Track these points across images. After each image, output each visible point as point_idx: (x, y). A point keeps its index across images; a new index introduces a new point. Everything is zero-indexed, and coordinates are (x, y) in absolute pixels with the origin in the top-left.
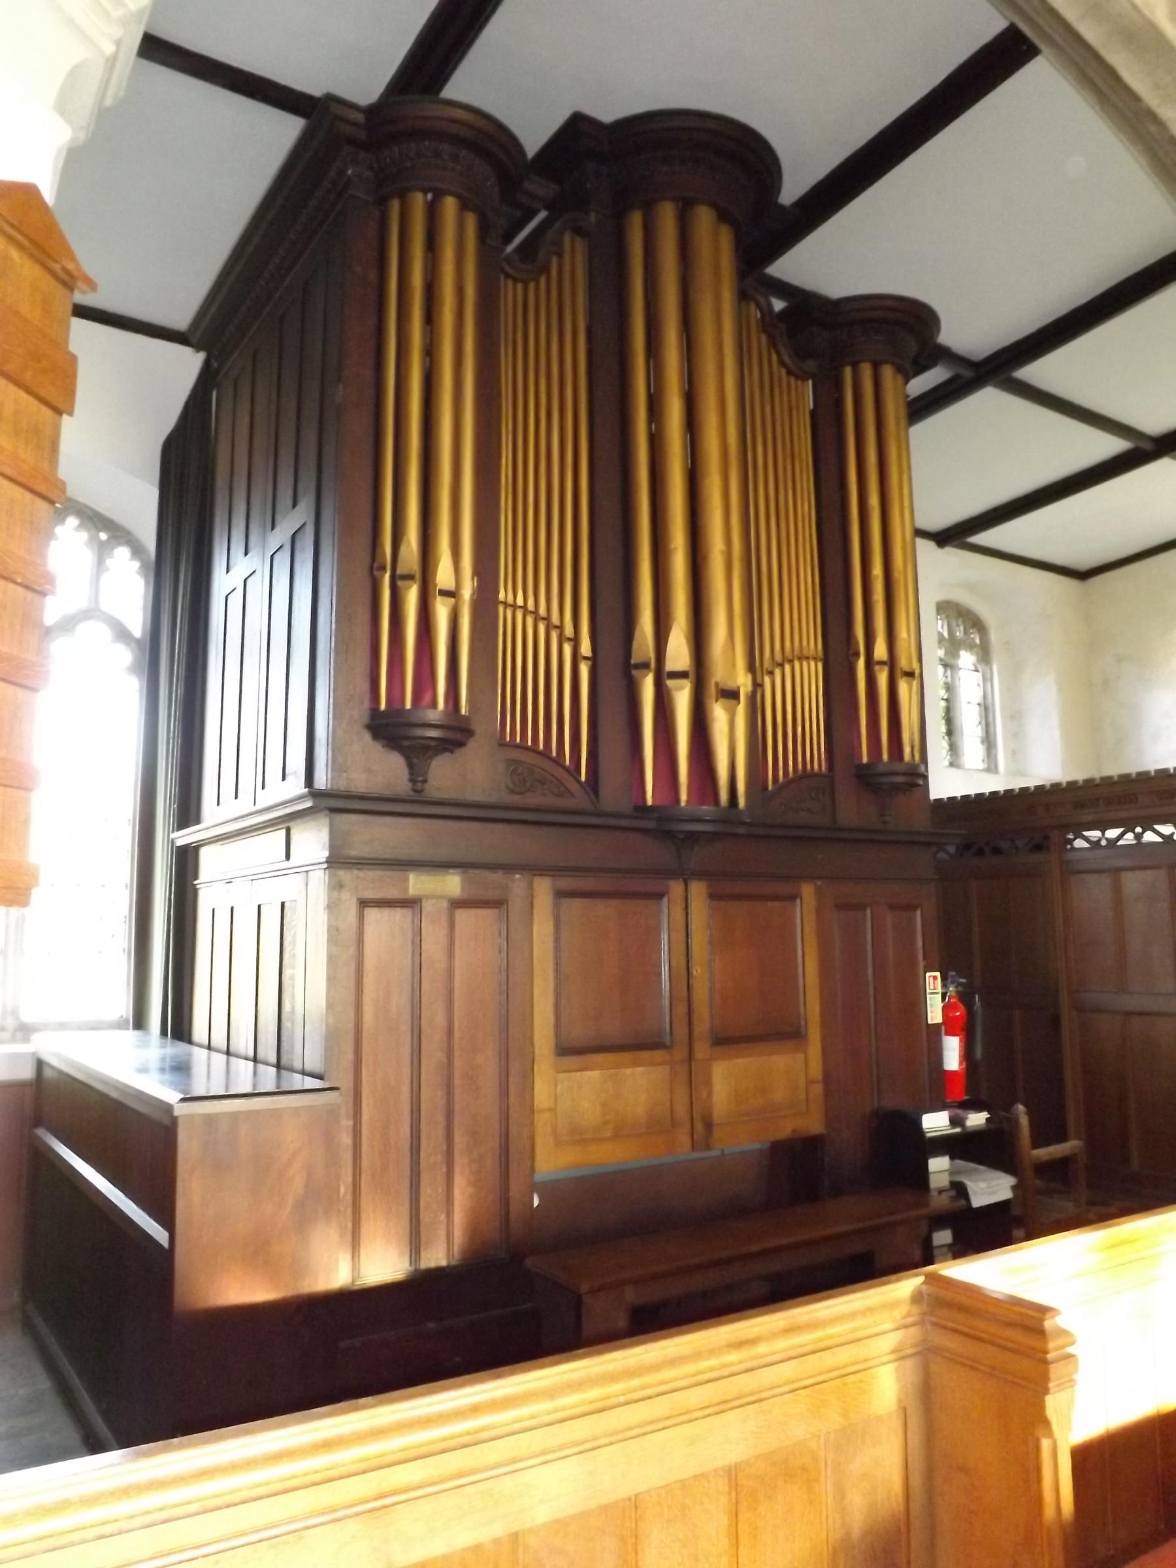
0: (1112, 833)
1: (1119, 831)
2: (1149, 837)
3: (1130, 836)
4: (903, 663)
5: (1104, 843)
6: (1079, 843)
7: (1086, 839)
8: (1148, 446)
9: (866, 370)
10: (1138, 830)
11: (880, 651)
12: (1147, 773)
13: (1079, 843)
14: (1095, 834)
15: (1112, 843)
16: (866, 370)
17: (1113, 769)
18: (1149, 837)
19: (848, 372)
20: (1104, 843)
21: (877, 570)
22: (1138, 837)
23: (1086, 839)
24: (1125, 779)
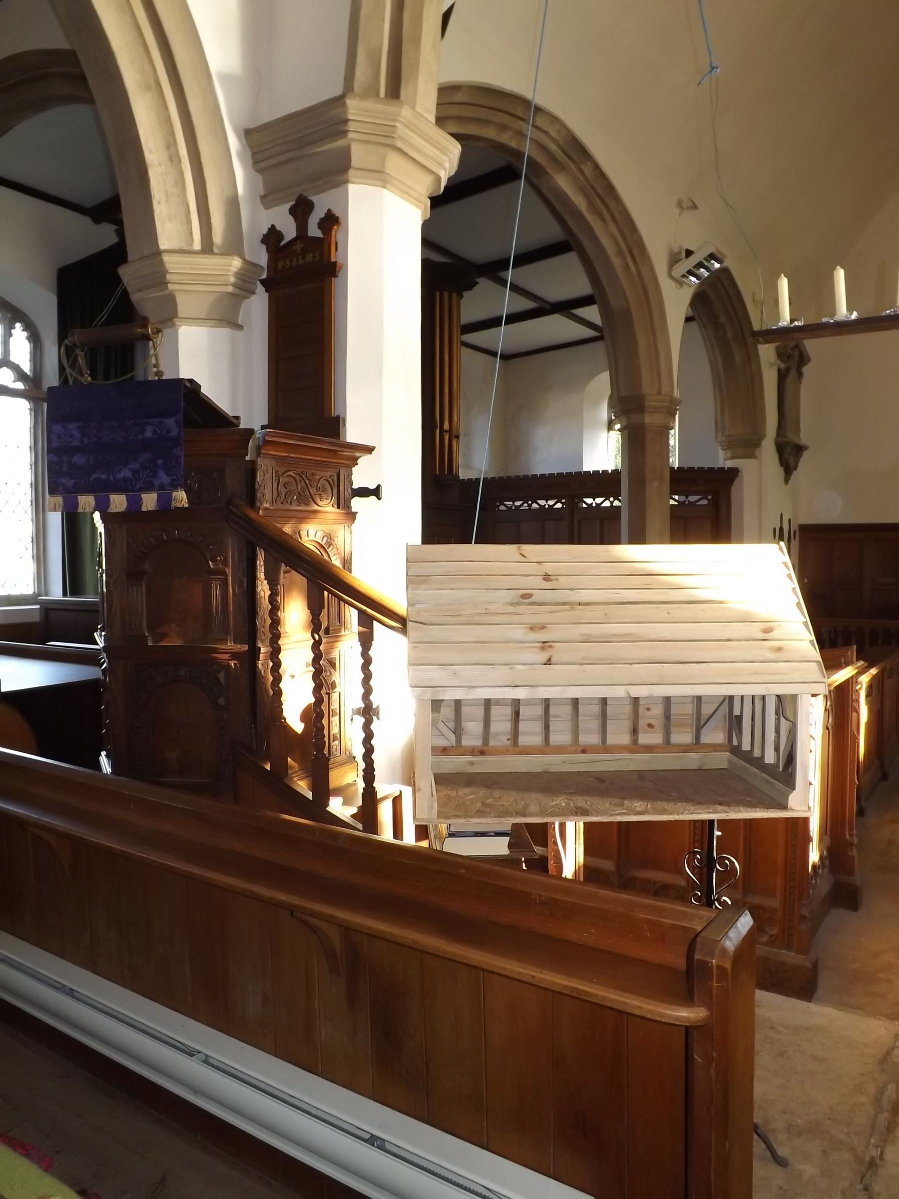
0: (518, 503)
1: (698, 497)
2: (535, 506)
3: (526, 505)
4: (454, 431)
5: (594, 505)
6: (502, 508)
7: (505, 506)
8: (547, 306)
9: (446, 294)
10: (612, 499)
11: (446, 426)
12: (519, 476)
13: (502, 508)
14: (542, 502)
15: (518, 507)
16: (446, 294)
17: (512, 473)
18: (535, 506)
19: (438, 293)
20: (594, 505)
21: (446, 390)
22: (530, 506)
23: (505, 506)
24: (518, 478)
